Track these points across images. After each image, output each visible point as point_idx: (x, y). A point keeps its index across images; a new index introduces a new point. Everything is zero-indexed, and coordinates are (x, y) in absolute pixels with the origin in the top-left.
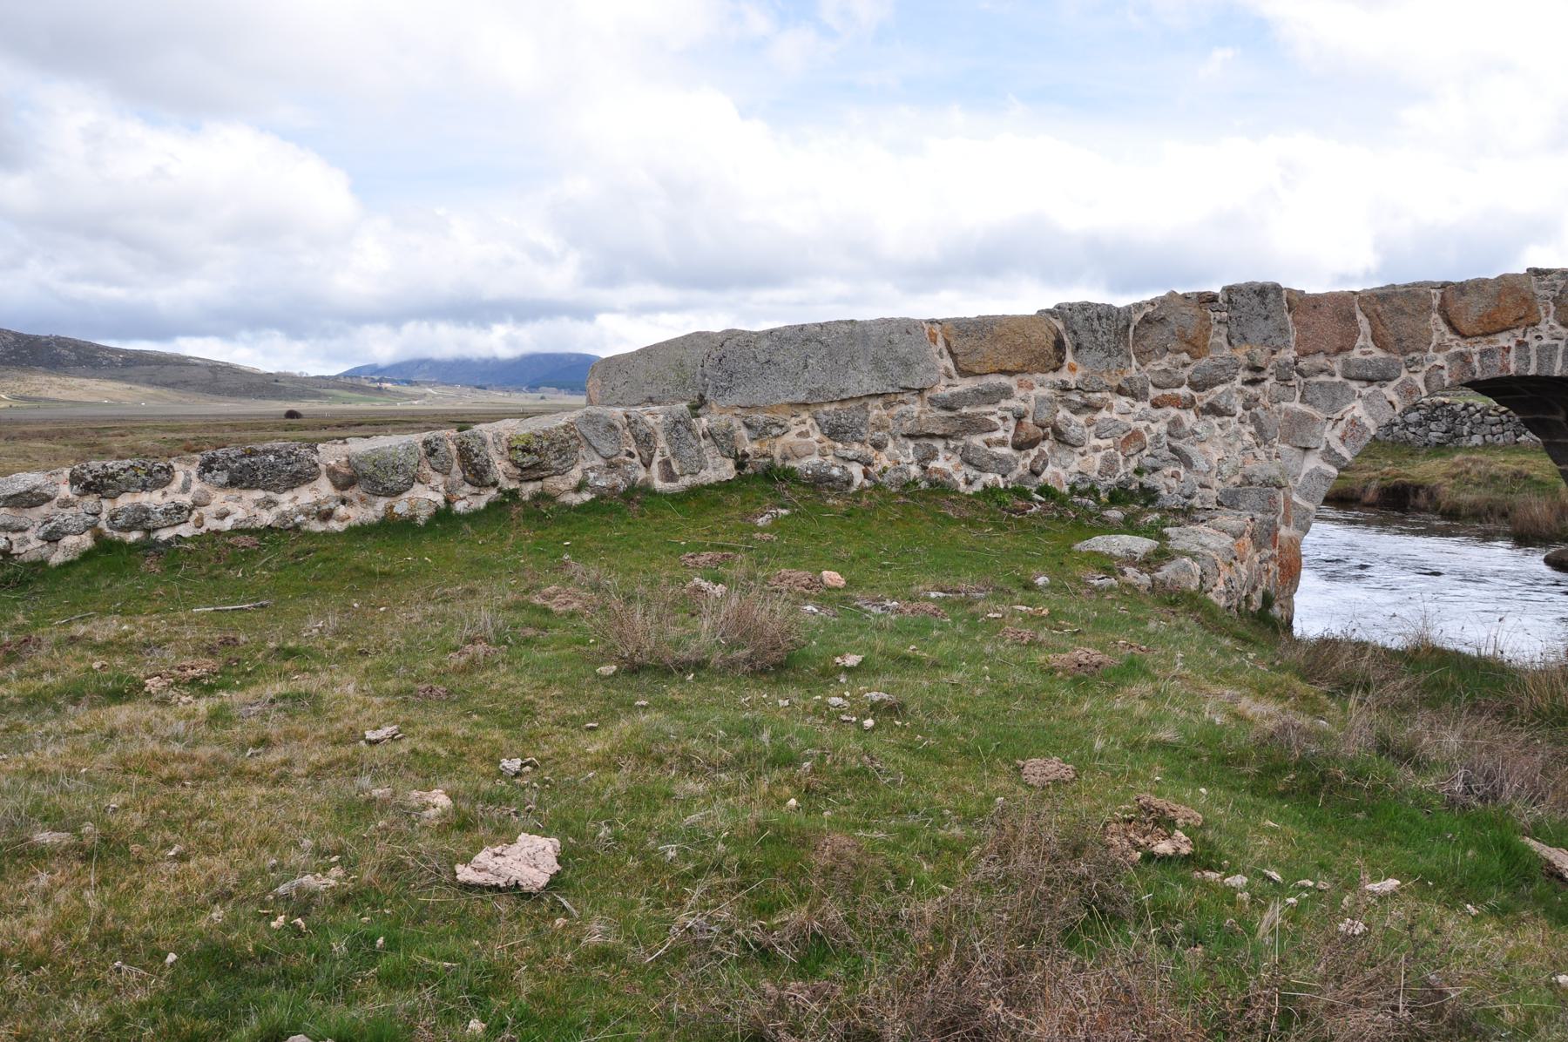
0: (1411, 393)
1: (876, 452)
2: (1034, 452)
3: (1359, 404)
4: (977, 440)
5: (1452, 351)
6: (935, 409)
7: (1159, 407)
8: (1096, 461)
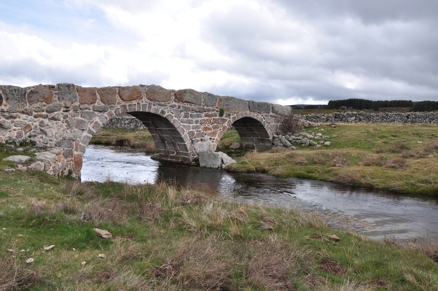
0: (111, 115)
3: (97, 118)
8: (15, 133)
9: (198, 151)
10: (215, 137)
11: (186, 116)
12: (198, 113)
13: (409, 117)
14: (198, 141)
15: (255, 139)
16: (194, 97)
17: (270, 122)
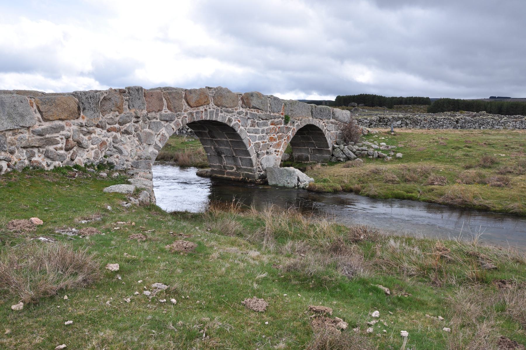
0: (178, 125)
1: (11, 155)
2: (72, 152)
3: (164, 129)
4: (51, 148)
5: (189, 112)
6: (35, 136)
7: (110, 132)
8: (92, 153)
9: (265, 167)
10: (280, 149)
11: (252, 125)
12: (265, 121)
13: (459, 122)
14: (264, 154)
15: (311, 149)
16: (262, 102)
17: (330, 130)
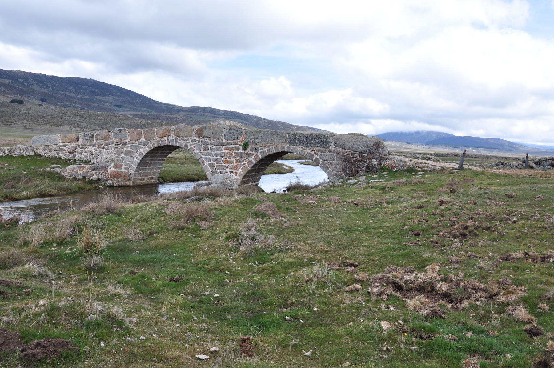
10: (238, 170)
